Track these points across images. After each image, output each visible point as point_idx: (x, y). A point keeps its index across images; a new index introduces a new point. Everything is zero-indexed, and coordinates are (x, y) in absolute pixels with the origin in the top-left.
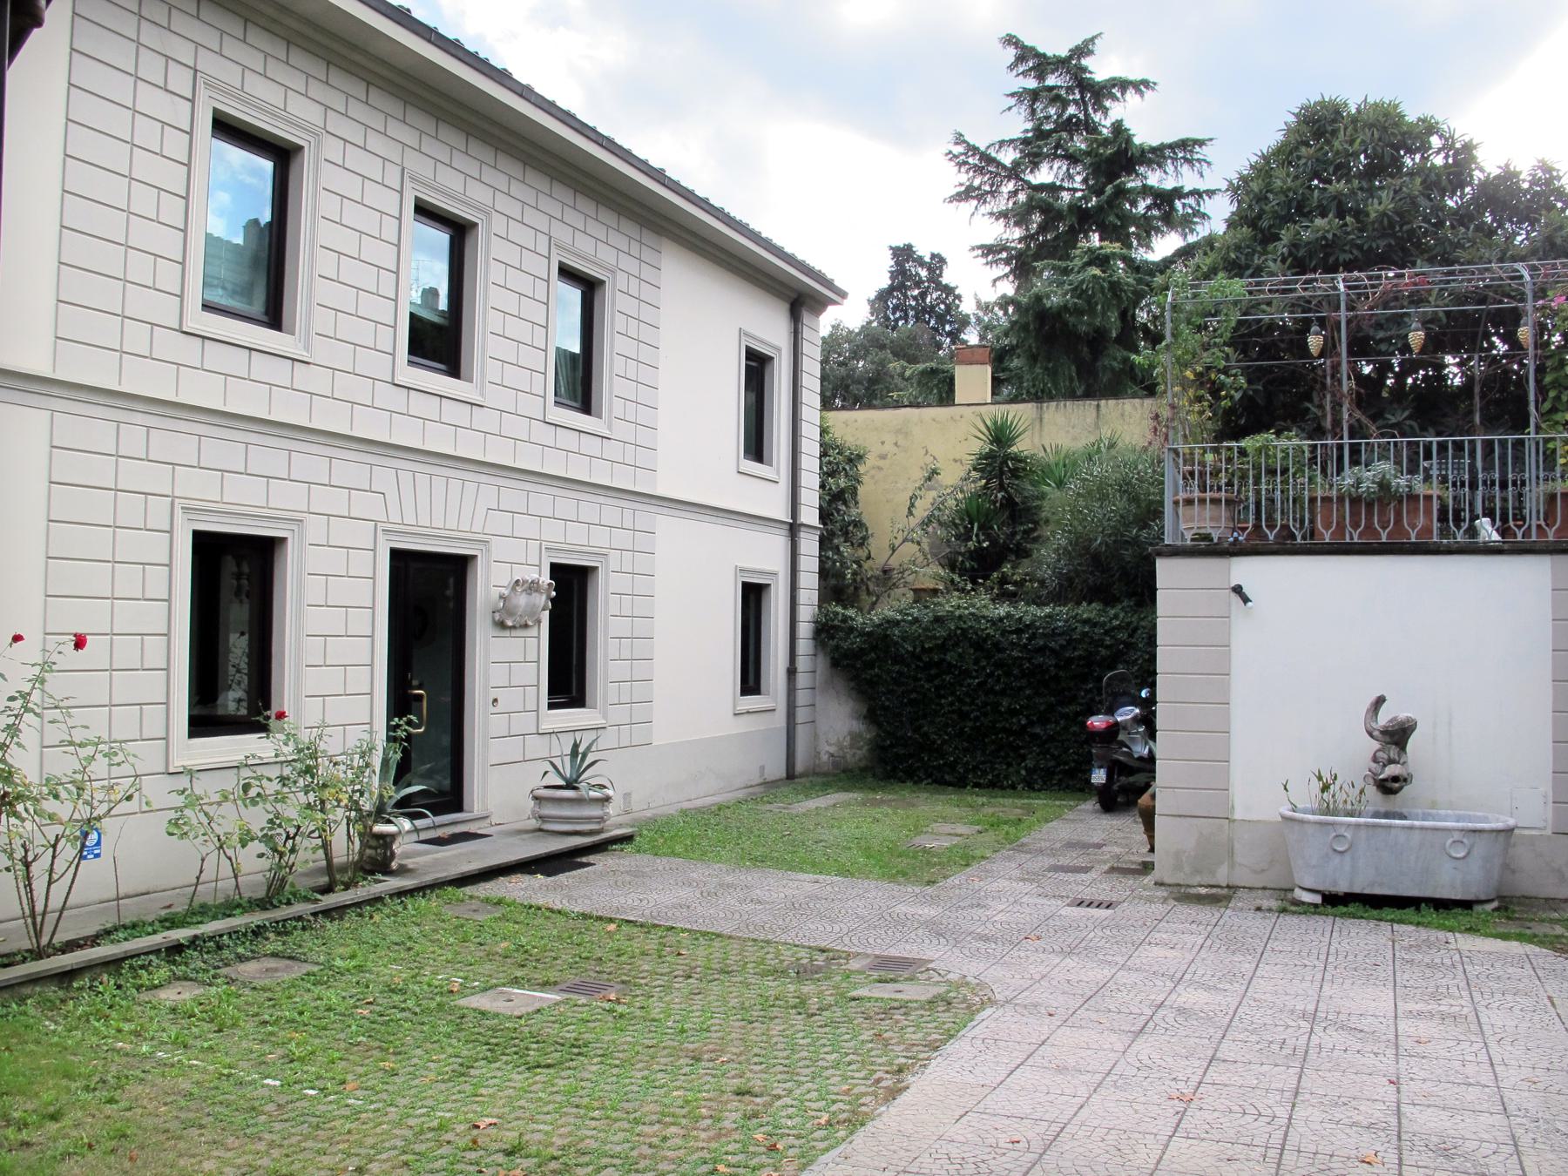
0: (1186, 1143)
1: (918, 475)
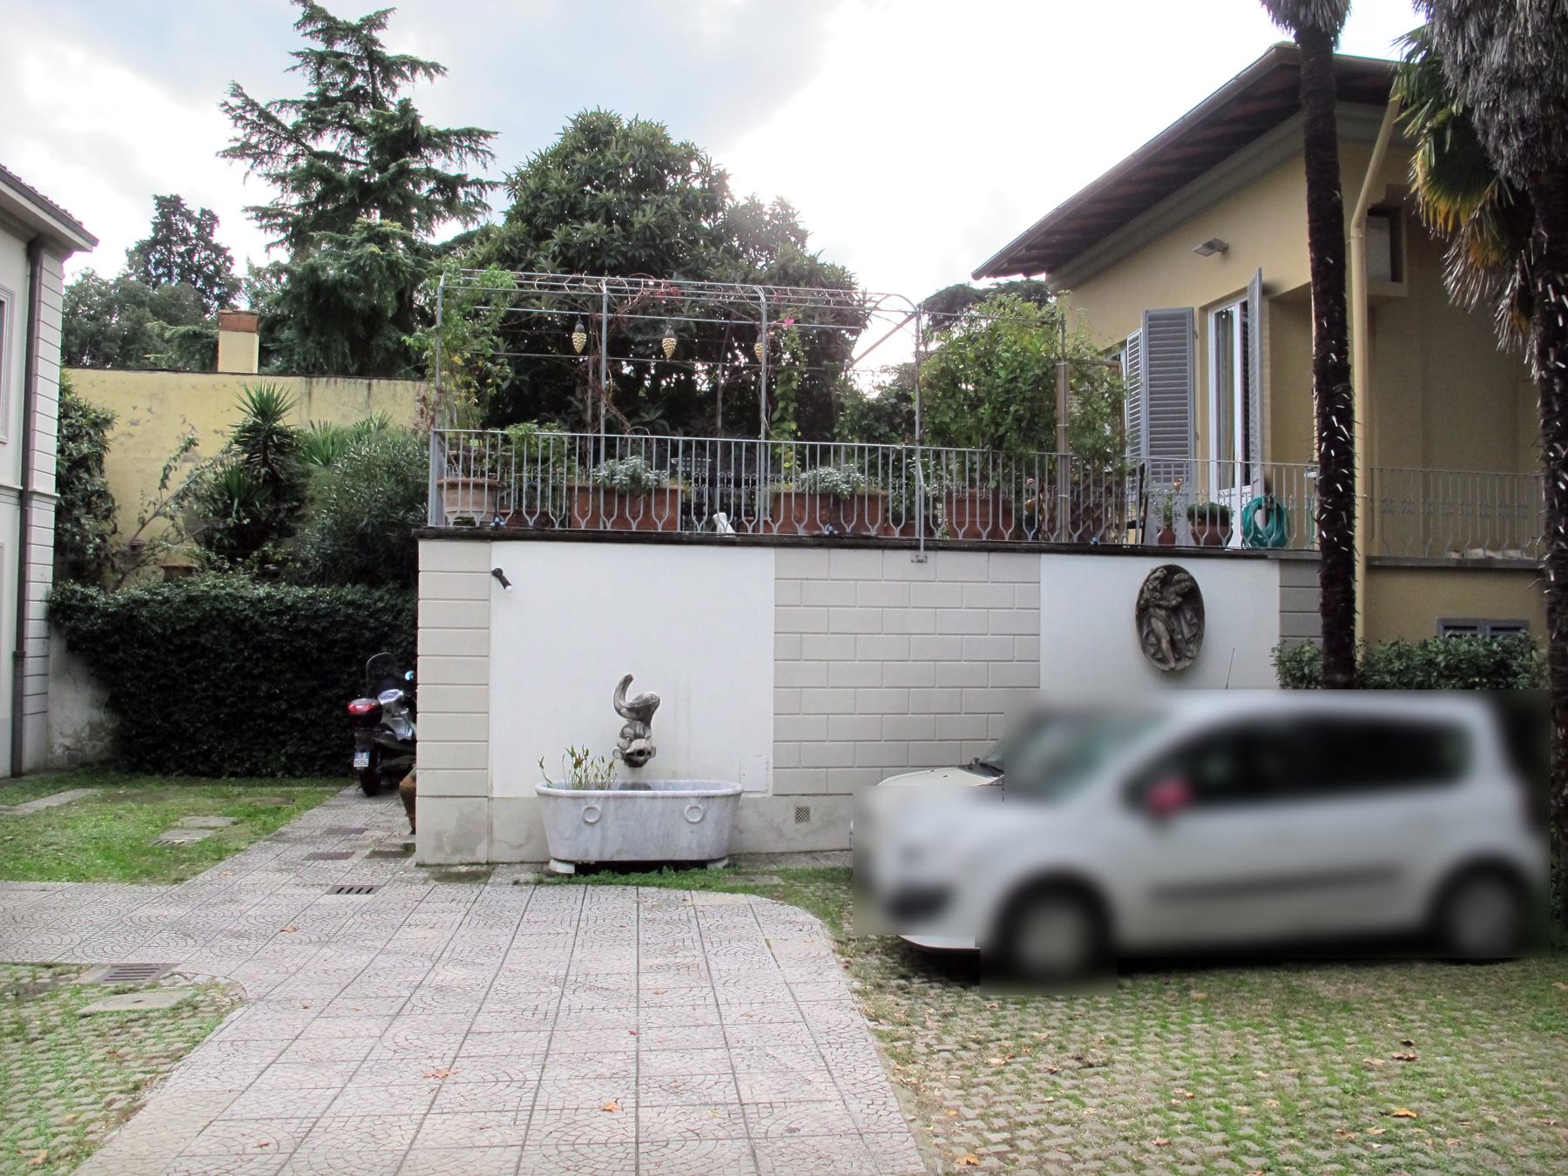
0: (438, 1119)
1: (175, 445)
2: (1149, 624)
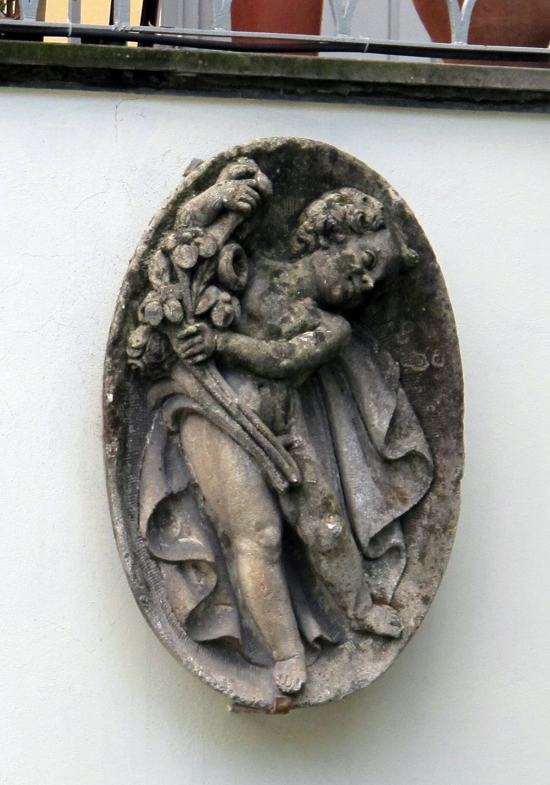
2: (172, 454)
